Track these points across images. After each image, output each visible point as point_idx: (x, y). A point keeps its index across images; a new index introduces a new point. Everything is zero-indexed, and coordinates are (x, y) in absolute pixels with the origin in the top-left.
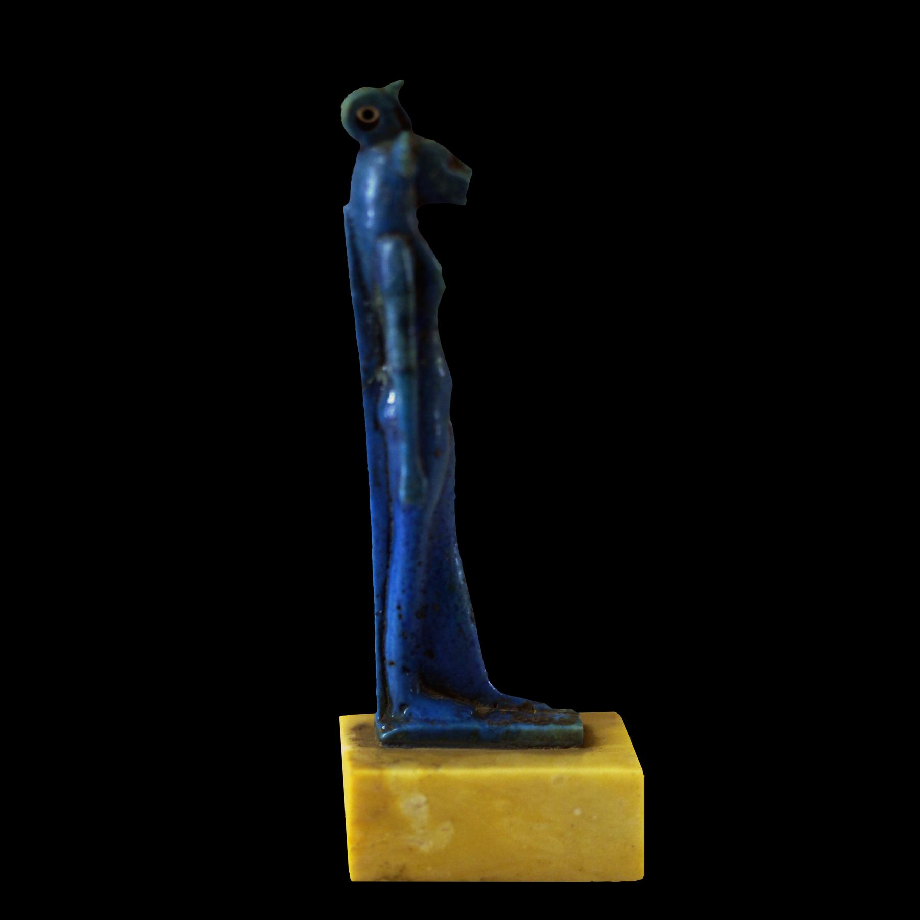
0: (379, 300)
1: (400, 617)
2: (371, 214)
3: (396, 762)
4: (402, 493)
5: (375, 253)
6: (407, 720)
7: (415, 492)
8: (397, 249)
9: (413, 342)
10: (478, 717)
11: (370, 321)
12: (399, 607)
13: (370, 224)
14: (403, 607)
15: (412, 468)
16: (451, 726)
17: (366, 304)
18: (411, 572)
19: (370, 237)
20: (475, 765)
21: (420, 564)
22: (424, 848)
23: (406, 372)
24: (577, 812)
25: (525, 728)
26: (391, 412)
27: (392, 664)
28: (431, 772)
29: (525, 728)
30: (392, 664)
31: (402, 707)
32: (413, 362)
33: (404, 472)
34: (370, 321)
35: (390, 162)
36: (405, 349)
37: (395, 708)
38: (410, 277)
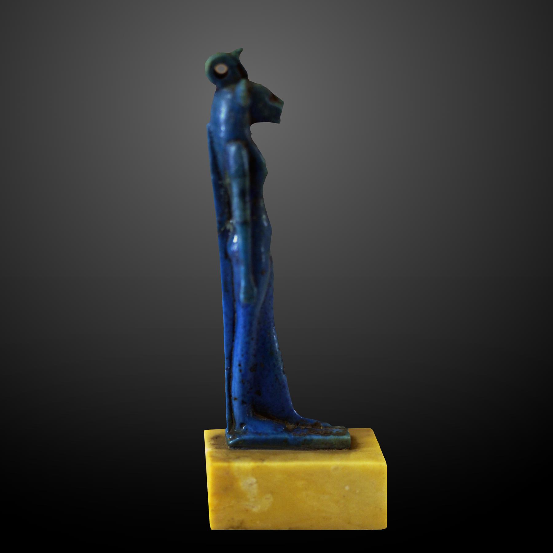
0: (228, 181)
1: (240, 371)
2: (223, 128)
3: (238, 458)
4: (242, 296)
5: (226, 152)
6: (245, 433)
7: (249, 296)
8: (239, 150)
9: (248, 206)
10: (287, 431)
11: (222, 193)
12: (240, 365)
13: (222, 135)
14: (242, 365)
15: (248, 281)
16: (271, 437)
17: (220, 183)
18: (247, 344)
19: (223, 143)
20: (285, 460)
21: (252, 339)
22: (255, 510)
23: (244, 223)
24: (347, 488)
25: (316, 437)
26: (235, 248)
27: (235, 399)
28: (259, 464)
29: (316, 437)
30: (235, 399)
31: (242, 425)
32: (249, 218)
33: (243, 283)
34: (222, 193)
35: (234, 98)
36: (244, 210)
37: (237, 426)
38: (247, 166)
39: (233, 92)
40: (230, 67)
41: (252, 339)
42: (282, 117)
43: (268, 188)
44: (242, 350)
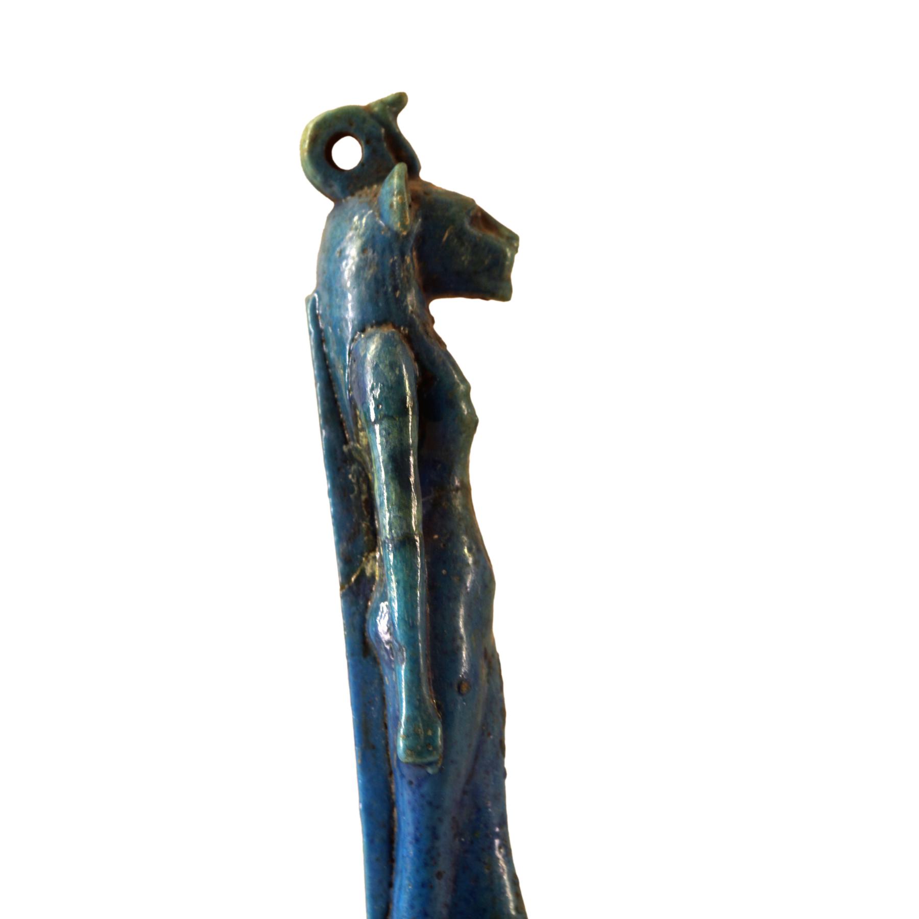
5: (357, 359)
7: (421, 745)
18: (424, 888)
21: (439, 875)
39: (375, 204)
40: (368, 142)
41: (439, 875)
42: (518, 276)
43: (493, 477)
44: (412, 907)
